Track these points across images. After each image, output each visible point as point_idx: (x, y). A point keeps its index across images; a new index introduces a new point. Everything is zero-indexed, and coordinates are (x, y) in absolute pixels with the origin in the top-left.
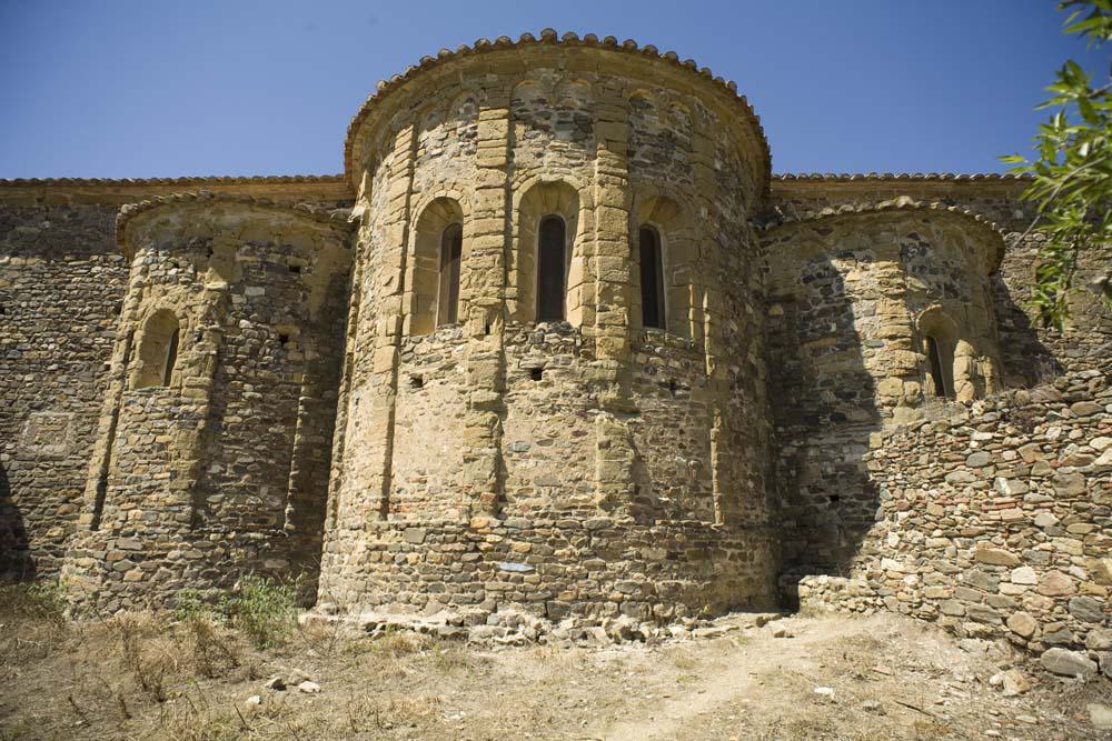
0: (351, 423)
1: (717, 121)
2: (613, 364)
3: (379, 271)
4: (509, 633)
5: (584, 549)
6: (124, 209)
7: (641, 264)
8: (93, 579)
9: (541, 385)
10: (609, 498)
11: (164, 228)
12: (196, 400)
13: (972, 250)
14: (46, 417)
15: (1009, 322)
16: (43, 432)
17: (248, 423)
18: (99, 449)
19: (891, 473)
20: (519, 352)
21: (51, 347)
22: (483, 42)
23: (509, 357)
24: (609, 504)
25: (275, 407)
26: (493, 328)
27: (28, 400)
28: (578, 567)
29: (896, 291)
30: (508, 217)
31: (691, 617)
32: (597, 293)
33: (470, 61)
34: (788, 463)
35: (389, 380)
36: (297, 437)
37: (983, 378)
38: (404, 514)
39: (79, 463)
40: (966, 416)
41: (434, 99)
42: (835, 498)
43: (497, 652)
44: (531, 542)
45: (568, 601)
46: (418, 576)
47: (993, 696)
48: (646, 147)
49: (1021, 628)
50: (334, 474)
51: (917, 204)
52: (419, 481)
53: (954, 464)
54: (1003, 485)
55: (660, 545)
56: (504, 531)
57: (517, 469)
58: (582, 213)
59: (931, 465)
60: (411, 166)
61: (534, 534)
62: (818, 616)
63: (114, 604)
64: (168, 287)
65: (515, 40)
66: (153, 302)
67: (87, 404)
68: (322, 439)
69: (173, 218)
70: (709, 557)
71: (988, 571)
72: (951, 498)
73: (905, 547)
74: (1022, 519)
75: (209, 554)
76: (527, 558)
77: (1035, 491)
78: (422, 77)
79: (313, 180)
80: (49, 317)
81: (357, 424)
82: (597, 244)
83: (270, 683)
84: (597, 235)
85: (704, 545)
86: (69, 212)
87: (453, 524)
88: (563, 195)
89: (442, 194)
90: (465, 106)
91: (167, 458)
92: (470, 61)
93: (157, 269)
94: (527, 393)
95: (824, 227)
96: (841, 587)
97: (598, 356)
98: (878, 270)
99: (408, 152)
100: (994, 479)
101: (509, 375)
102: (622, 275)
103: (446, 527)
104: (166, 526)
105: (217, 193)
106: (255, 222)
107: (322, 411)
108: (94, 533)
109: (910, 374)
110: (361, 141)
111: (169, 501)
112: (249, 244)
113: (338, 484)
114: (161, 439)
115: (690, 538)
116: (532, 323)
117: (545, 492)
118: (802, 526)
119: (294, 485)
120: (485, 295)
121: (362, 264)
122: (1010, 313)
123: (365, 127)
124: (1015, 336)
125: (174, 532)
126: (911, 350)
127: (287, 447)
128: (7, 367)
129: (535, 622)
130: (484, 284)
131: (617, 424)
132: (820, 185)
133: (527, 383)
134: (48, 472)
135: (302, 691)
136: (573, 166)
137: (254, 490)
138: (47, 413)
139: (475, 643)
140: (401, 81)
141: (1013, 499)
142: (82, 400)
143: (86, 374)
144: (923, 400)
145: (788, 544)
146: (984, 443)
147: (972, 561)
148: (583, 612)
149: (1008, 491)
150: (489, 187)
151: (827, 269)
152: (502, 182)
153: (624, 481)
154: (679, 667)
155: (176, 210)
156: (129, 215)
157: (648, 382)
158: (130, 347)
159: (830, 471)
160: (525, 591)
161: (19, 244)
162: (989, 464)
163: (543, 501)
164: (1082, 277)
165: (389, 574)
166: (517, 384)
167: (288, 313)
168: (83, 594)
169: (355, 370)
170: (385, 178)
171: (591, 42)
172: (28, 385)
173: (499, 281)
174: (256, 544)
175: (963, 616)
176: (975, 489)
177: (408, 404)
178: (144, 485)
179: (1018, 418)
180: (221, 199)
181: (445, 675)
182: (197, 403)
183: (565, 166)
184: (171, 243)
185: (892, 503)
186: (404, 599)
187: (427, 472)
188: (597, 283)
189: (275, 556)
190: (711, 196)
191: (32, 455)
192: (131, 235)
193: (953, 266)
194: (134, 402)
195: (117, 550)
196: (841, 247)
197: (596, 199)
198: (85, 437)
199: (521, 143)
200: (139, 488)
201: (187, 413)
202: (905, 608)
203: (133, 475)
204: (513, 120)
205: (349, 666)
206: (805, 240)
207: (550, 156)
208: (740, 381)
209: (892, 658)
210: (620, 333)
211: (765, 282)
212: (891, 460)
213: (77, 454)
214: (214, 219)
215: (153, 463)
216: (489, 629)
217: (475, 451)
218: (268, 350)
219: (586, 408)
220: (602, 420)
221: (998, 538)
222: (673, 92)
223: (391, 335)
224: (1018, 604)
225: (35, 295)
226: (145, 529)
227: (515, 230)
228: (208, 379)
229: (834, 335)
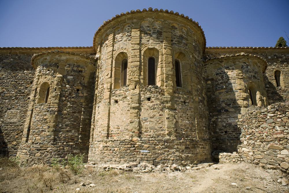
0: (97, 113)
1: (193, 32)
2: (169, 96)
3: (104, 72)
4: (144, 169)
5: (163, 146)
6: (34, 55)
7: (176, 70)
8: (27, 156)
9: (150, 102)
10: (169, 132)
11: (45, 60)
12: (55, 107)
13: (259, 66)
14: (11, 112)
15: (268, 86)
16: (11, 116)
17: (69, 113)
18: (27, 120)
19: (244, 125)
20: (144, 93)
21: (13, 92)
22: (133, 11)
23: (142, 95)
24: (169, 134)
25: (76, 108)
26: (137, 87)
27: (7, 107)
28: (162, 151)
29: (241, 77)
30: (140, 57)
31: (192, 164)
32: (165, 77)
33: (129, 16)
34: (213, 123)
35: (108, 101)
36: (82, 117)
37: (264, 100)
38: (113, 137)
39: (21, 124)
40: (266, 109)
41: (119, 26)
42: (226, 132)
43: (141, 175)
44: (149, 144)
45: (159, 160)
46: (118, 154)
47: (280, 186)
48: (176, 39)
49: (284, 167)
50: (92, 127)
51: (246, 54)
52: (118, 128)
53: (263, 122)
54: (277, 128)
55: (183, 145)
56: (141, 142)
57: (144, 125)
58: (160, 56)
59: (256, 123)
60: (113, 44)
61: (150, 142)
62: (224, 163)
63: (33, 162)
64: (46, 76)
65: (141, 10)
66: (42, 80)
67: (23, 108)
68: (89, 117)
69: (48, 58)
70: (195, 148)
71: (274, 151)
72: (262, 131)
73: (249, 145)
74: (283, 137)
75: (59, 149)
76: (148, 149)
77: (287, 130)
78: (116, 20)
79: (84, 48)
80: (12, 84)
81: (99, 113)
82: (164, 65)
83: (82, 184)
84: (164, 62)
85: (194, 145)
86: (18, 56)
87: (127, 140)
88: (154, 51)
89: (122, 51)
90: (128, 28)
91: (47, 122)
92: (129, 16)
93: (43, 71)
94: (146, 104)
95: (221, 60)
96: (230, 156)
97: (165, 94)
98: (236, 72)
99: (112, 40)
100: (275, 126)
101: (142, 100)
102: (171, 73)
103: (126, 141)
104: (47, 141)
105: (60, 51)
106: (70, 59)
107: (88, 110)
108: (27, 143)
109: (245, 99)
110: (98, 37)
111: (47, 134)
112: (68, 65)
113: (93, 129)
114: (45, 117)
115: (190, 143)
116: (147, 86)
117: (152, 131)
118: (217, 139)
119: (81, 130)
120: (135, 78)
121: (99, 70)
122: (268, 83)
124: (269, 89)
125: (49, 143)
126: (245, 93)
127: (79, 119)
128: (1, 98)
129: (151, 166)
130: (134, 75)
131: (171, 113)
132: (218, 50)
133: (147, 102)
134: (12, 127)
135: (91, 186)
136: (157, 44)
137: (70, 131)
138: (12, 110)
139: (135, 172)
140: (110, 21)
141: (281, 132)
142: (22, 107)
143: (23, 100)
144: (249, 106)
145: (214, 144)
146: (271, 117)
147: (269, 148)
148: (163, 163)
149: (279, 130)
150: (135, 49)
151: (222, 71)
152: (139, 48)
153: (173, 128)
154: (192, 178)
155: (49, 56)
156: (36, 57)
157: (178, 101)
158: (36, 93)
159: (224, 125)
160: (148, 158)
161: (4, 65)
162: (273, 122)
163: (152, 133)
164: (286, 74)
165: (110, 154)
166: (144, 102)
167: (79, 83)
168: (24, 160)
169: (97, 99)
170: (105, 47)
171: (161, 11)
172: (7, 103)
173: (138, 74)
174: (72, 146)
175: (267, 163)
176: (269, 129)
177: (114, 107)
178: (41, 130)
179: (281, 110)
180: (61, 53)
181: (129, 181)
182: (55, 108)
183: (155, 44)
184: (47, 64)
185: (245, 133)
186: (114, 160)
188: (165, 75)
189: (76, 149)
190: (193, 52)
191: (8, 122)
192: (35, 62)
193: (255, 71)
194: (37, 107)
195: (33, 148)
196: (226, 66)
197: (164, 53)
198: (23, 117)
199: (143, 38)
200: (39, 131)
201: (52, 110)
202: (249, 161)
203: (37, 127)
204: (141, 32)
205: (101, 179)
206: (216, 64)
207: (151, 41)
208: (201, 101)
209: (248, 175)
210: (171, 88)
211: (206, 75)
212: (244, 122)
213: (20, 122)
214: (59, 58)
215: (43, 124)
216: (139, 168)
217: (133, 120)
218: (74, 93)
219: (163, 108)
220: (167, 111)
221: (276, 142)
222: (182, 25)
223: (109, 89)
224: (283, 160)
225: (8, 79)
226: (41, 142)
227: (142, 60)
228: (58, 101)
229: (225, 89)
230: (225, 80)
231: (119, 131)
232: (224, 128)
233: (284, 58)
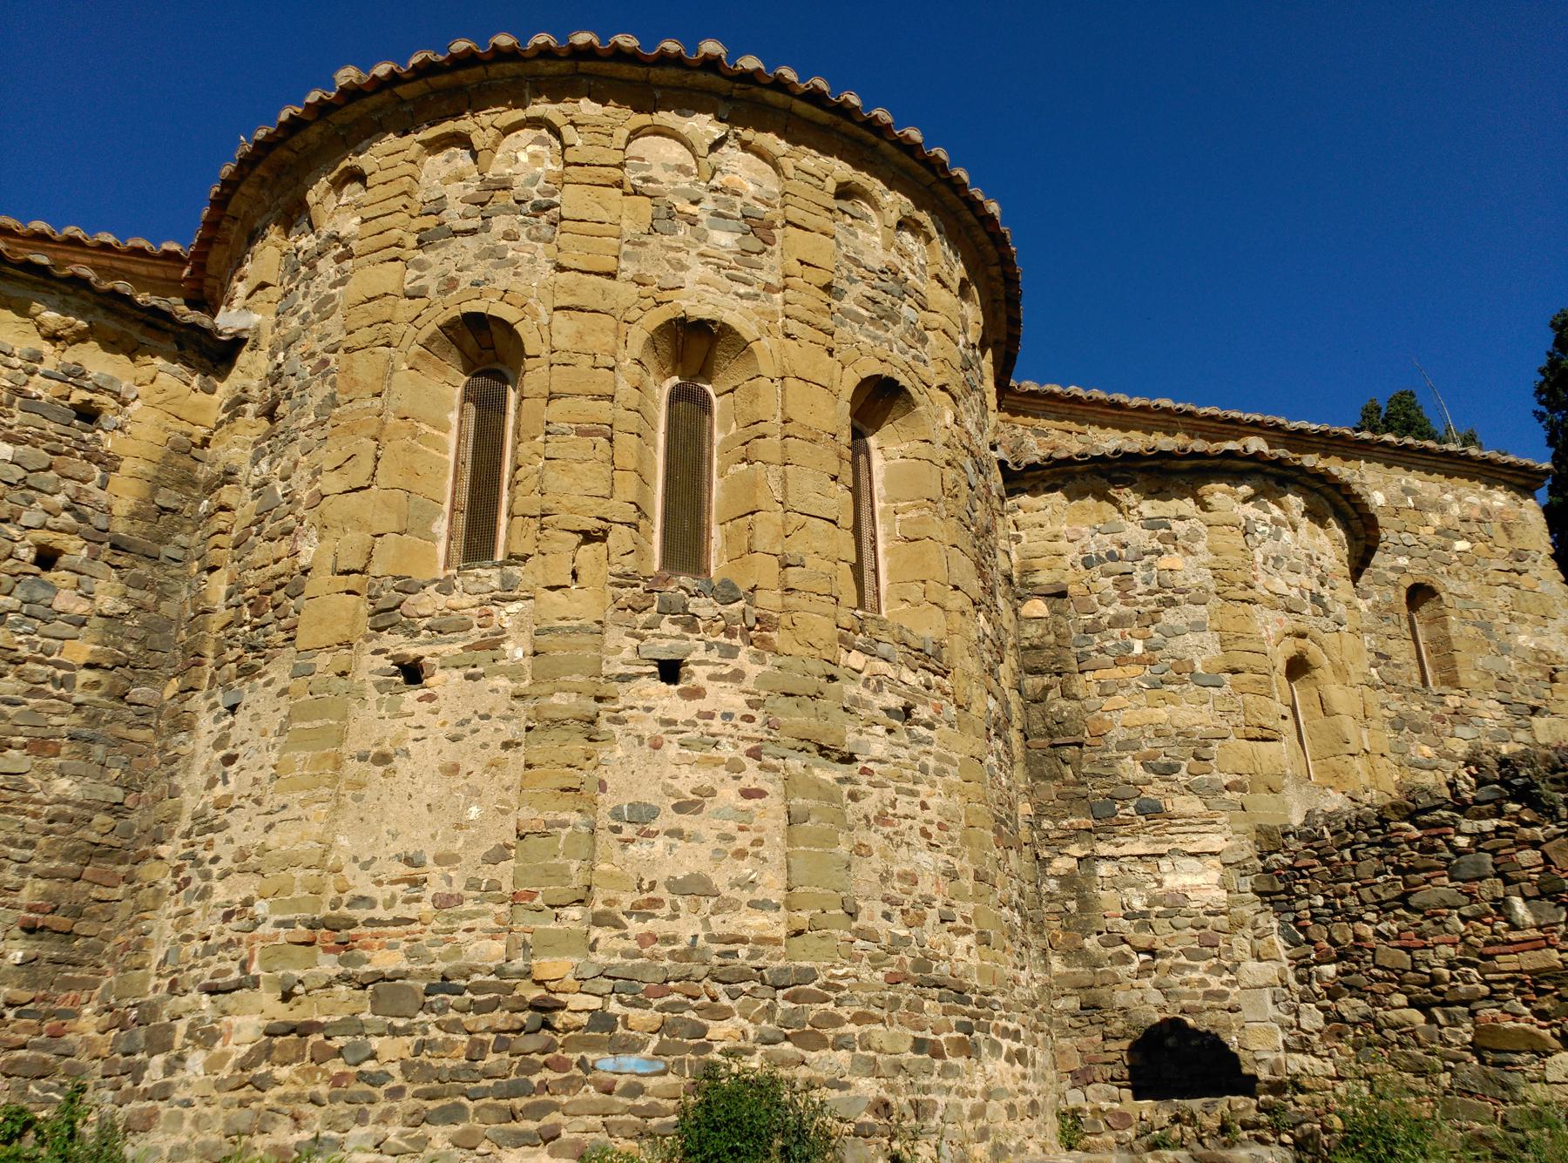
44: (661, 1009)
59: (1380, 879)
110: (264, 180)
118: (1091, 1007)
123: (283, 154)
151: (1124, 546)
159: (1138, 905)
187: (429, 861)
229: (1139, 661)
230: (1144, 604)
231: (418, 900)
232: (1138, 929)
233: (1455, 510)
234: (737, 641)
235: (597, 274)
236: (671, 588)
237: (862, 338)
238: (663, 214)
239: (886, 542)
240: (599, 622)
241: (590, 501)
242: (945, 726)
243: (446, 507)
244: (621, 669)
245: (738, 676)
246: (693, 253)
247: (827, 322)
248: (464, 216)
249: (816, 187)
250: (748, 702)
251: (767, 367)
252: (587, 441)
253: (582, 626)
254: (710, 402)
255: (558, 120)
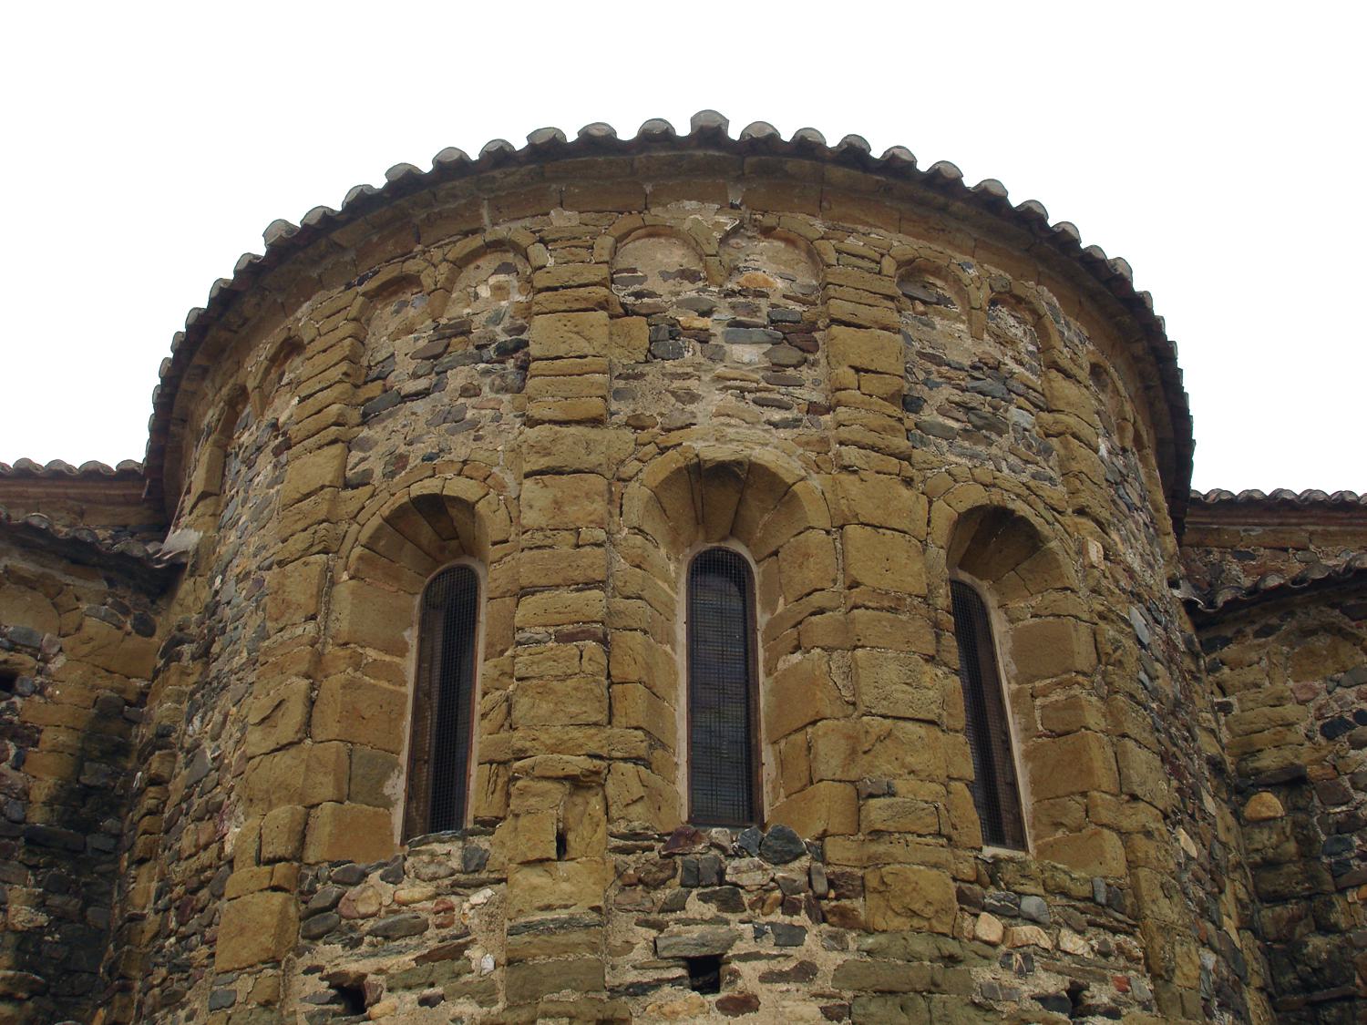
90: (492, 280)
206: (1313, 632)
234: (802, 919)
235: (579, 422)
236: (699, 847)
237: (953, 458)
238: (664, 333)
239: (1024, 741)
240: (597, 909)
241: (576, 733)
242: (1136, 1010)
243: (404, 758)
244: (632, 977)
245: (805, 971)
246: (706, 378)
247: (901, 443)
248: (415, 376)
249: (869, 271)
250: (824, 1010)
251: (816, 514)
252: (571, 648)
253: (572, 918)
254: (750, 571)
255: (523, 239)
